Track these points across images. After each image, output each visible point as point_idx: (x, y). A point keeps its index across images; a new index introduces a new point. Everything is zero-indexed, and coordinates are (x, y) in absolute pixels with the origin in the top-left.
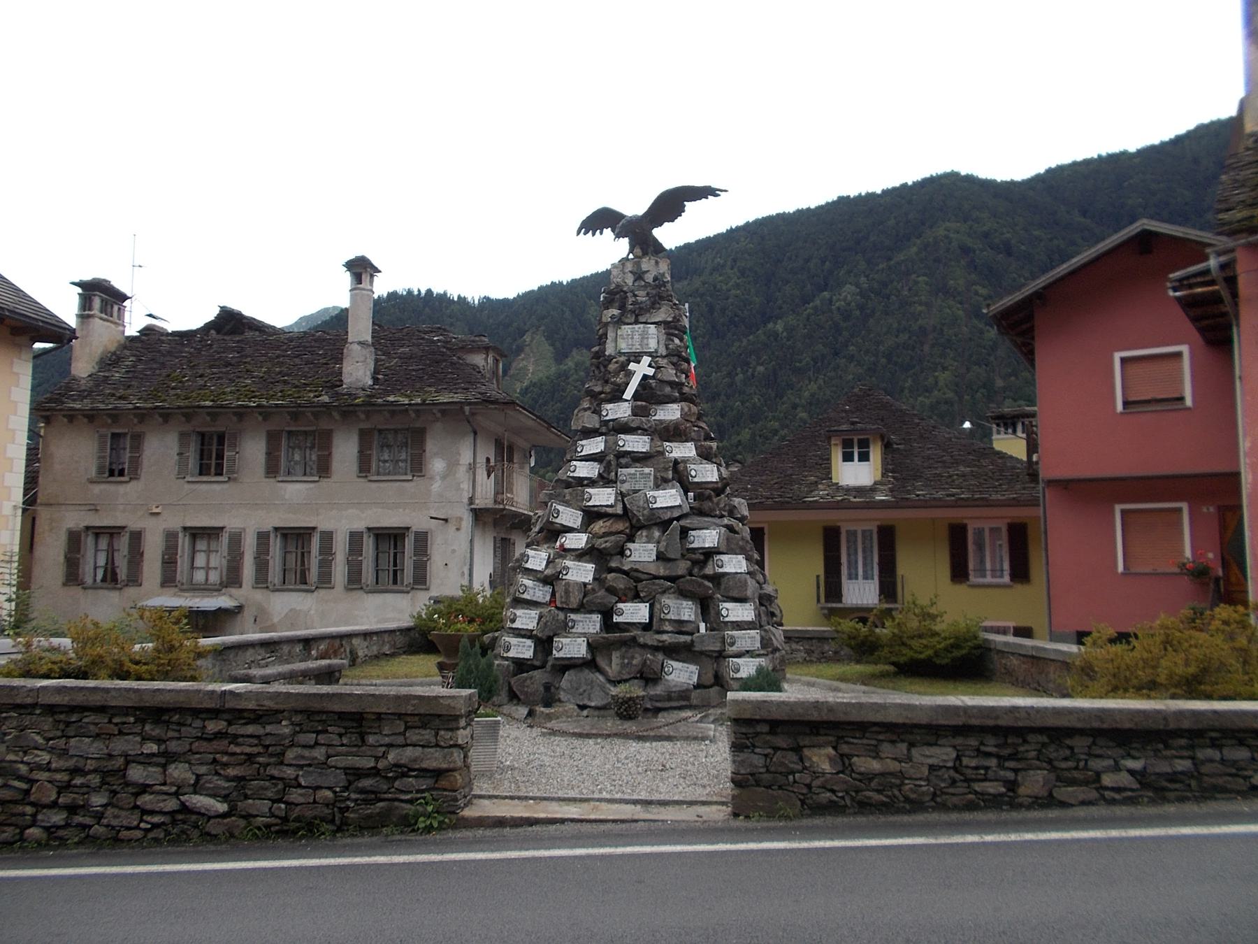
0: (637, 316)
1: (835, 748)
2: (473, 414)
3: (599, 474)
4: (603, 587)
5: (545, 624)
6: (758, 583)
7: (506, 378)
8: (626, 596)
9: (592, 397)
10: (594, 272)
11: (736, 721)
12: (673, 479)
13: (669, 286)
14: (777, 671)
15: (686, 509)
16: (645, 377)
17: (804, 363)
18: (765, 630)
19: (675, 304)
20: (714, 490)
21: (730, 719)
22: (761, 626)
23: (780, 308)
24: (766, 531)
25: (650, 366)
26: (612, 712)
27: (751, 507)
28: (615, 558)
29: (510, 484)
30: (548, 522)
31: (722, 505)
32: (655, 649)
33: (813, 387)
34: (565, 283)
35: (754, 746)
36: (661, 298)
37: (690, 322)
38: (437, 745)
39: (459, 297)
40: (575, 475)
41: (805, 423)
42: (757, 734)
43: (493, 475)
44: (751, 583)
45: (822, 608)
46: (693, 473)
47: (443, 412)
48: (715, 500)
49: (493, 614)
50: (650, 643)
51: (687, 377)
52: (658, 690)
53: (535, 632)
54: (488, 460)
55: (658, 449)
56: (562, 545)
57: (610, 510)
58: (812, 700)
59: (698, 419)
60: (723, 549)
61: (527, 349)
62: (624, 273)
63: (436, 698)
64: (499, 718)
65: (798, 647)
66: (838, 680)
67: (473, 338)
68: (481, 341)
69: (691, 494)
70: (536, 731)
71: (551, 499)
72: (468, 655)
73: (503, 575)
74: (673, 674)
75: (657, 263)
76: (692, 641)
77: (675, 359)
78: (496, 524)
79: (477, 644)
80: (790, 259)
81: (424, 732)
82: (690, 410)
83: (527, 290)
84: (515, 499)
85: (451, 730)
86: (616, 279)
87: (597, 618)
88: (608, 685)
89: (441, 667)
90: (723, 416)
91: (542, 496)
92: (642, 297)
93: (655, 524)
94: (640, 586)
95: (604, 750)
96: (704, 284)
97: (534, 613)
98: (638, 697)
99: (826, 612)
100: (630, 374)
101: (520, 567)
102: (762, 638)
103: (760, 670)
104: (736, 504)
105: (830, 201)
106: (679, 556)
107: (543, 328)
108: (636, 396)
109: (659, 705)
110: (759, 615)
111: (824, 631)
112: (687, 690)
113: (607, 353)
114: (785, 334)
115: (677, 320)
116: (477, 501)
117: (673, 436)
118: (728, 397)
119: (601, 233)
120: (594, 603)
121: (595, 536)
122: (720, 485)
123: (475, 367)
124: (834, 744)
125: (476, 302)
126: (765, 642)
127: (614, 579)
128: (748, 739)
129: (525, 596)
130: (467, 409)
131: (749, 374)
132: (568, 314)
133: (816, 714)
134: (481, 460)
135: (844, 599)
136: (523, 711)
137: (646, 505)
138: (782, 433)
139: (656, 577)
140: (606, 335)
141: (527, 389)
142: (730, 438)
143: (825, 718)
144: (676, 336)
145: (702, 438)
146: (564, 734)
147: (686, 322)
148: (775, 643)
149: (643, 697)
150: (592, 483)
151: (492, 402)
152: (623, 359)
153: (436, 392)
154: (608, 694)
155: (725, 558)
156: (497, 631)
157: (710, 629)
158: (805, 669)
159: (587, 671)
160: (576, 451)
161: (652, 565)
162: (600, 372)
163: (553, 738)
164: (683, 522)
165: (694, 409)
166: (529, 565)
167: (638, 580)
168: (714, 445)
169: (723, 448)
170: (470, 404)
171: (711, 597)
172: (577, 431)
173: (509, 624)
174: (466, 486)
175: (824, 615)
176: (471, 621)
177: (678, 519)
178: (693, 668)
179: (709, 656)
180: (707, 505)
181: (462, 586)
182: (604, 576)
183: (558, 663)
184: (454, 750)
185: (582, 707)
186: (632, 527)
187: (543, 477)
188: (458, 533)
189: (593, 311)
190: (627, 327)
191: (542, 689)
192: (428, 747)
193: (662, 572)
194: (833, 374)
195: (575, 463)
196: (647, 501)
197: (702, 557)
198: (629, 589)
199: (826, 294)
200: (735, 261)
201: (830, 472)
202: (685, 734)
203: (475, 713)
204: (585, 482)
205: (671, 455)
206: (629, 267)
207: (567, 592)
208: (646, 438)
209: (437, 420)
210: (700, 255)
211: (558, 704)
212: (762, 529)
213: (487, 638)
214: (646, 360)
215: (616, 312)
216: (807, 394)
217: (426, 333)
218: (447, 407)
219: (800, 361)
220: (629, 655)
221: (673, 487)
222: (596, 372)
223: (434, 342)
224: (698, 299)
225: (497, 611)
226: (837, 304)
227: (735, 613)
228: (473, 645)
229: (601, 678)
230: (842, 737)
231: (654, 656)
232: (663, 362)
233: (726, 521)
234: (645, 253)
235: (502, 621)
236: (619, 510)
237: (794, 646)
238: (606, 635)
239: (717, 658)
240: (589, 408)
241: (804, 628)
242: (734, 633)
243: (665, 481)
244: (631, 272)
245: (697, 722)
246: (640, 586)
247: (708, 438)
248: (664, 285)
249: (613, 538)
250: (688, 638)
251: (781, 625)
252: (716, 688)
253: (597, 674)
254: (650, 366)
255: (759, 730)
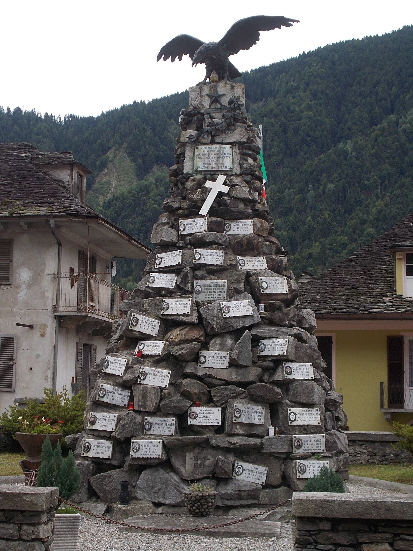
0: (213, 137)
1: (391, 544)
2: (58, 227)
3: (177, 285)
4: (179, 391)
5: (123, 426)
6: (324, 389)
7: (90, 192)
8: (200, 400)
9: (170, 212)
10: (174, 92)
11: (301, 519)
12: (245, 290)
13: (243, 109)
14: (340, 472)
15: (257, 320)
16: (220, 194)
17: (372, 180)
18: (330, 434)
19: (249, 126)
20: (284, 301)
21: (294, 517)
22: (327, 430)
23: (350, 129)
24: (334, 340)
25: (225, 184)
26: (185, 509)
27: (319, 317)
28: (190, 364)
29: (93, 292)
30: (127, 329)
31: (291, 316)
32: (227, 450)
33: (380, 204)
34: (146, 103)
35: (316, 542)
36: (236, 120)
37: (264, 141)
38: (20, 539)
39: (46, 115)
40: (154, 285)
41: (373, 237)
42: (320, 531)
43: (76, 285)
44: (318, 389)
45: (385, 413)
46: (264, 285)
47: (30, 225)
48: (285, 310)
49: (75, 416)
50: (222, 445)
51: (260, 194)
52: (229, 489)
53: (113, 434)
54: (72, 270)
55: (232, 262)
56: (140, 352)
57: (186, 319)
58: (371, 500)
59: (270, 234)
60: (292, 356)
61: (110, 165)
62: (201, 97)
63: (19, 495)
64: (79, 515)
65: (361, 450)
66: (397, 481)
67: (58, 155)
68: (67, 158)
69: (262, 305)
70: (113, 527)
71: (130, 308)
72: (50, 455)
73: (84, 379)
74: (243, 475)
75: (232, 87)
76: (261, 443)
77: (248, 178)
78: (79, 330)
79: (59, 445)
80: (359, 83)
81: (7, 526)
82: (262, 225)
83: (111, 109)
84: (97, 307)
85: (34, 525)
86: (194, 100)
87: (172, 421)
88: (182, 485)
89: (25, 466)
90: (294, 230)
91: (122, 305)
92: (218, 118)
93: (229, 333)
94: (213, 391)
95: (177, 546)
96: (278, 105)
97: (113, 416)
98: (209, 495)
99: (389, 416)
100: (206, 191)
101: (100, 372)
102: (327, 441)
103: (324, 471)
104: (304, 314)
105: (396, 30)
106: (249, 363)
107: (125, 145)
108: (212, 212)
109: (229, 503)
110: (325, 419)
111: (387, 435)
112: (256, 489)
113: (185, 171)
114: (354, 153)
115: (251, 140)
116: (61, 309)
117: (246, 250)
118: (300, 213)
119: (180, 59)
120: (170, 407)
121: (172, 343)
122: (289, 297)
123: (60, 182)
124: (391, 541)
125: (63, 119)
126: (330, 445)
127: (188, 385)
128: (311, 535)
129: (105, 400)
130: (52, 221)
131: (320, 191)
132: (149, 133)
133: (374, 513)
134: (65, 270)
135: (406, 404)
136: (101, 508)
137: (219, 314)
138: (350, 246)
139: (228, 383)
140: (183, 154)
141: (110, 202)
142: (301, 251)
143: (383, 517)
144: (250, 156)
145: (273, 252)
146: (140, 529)
147: (260, 143)
148: (340, 446)
149: (215, 495)
150: (169, 293)
151: (76, 216)
152: (199, 177)
153: (23, 205)
154: (181, 493)
155: (293, 365)
156: (78, 432)
157: (278, 432)
158: (368, 471)
159: (162, 471)
160: (155, 263)
161: (225, 371)
162: (178, 189)
163: (129, 534)
164: (254, 331)
165: (266, 225)
166: (108, 371)
167: (212, 386)
168: (285, 259)
169: (295, 260)
170: (55, 217)
171: (280, 403)
172: (156, 244)
173: (89, 426)
174: (50, 294)
175: (387, 419)
176: (54, 422)
177: (250, 328)
178: (262, 469)
179: (276, 458)
180: (277, 315)
181: (45, 389)
182: (179, 381)
183: (135, 463)
184: (36, 543)
185: (157, 505)
186: (207, 335)
187: (124, 286)
188: (42, 339)
189: (173, 129)
190: (203, 147)
191: (119, 487)
192: (12, 540)
193: (234, 378)
194: (398, 192)
195: (153, 274)
196: (221, 310)
197: (272, 365)
198: (203, 393)
199: (393, 117)
200: (307, 84)
201: (394, 285)
202: (253, 531)
203: (56, 509)
204: (164, 292)
205: (243, 268)
206: (206, 90)
207: (144, 396)
208: (220, 252)
209: (24, 232)
210: (274, 79)
211: (134, 501)
212: (331, 337)
213: (68, 439)
214: (221, 178)
215: (193, 132)
216: (374, 210)
217: (14, 149)
218: (34, 220)
219: (369, 180)
220: (202, 456)
221: (245, 298)
222: (175, 189)
223: (22, 158)
224: (273, 120)
225: (78, 413)
226: (403, 126)
227: (302, 417)
228: (54, 445)
229: (176, 478)
230: (399, 534)
231: (226, 457)
232: (237, 180)
233: (295, 331)
234: (221, 78)
235: (83, 423)
236: (194, 318)
237: (358, 449)
238: (181, 438)
239: (285, 459)
240: (167, 223)
241: (367, 433)
242: (302, 436)
243: (238, 292)
244: (208, 95)
245: (265, 519)
246: (213, 391)
247: (279, 252)
248: (239, 107)
249: (188, 345)
250: (257, 441)
251: (347, 428)
252: (283, 488)
253: (172, 474)
254: (225, 184)
255: (321, 527)
